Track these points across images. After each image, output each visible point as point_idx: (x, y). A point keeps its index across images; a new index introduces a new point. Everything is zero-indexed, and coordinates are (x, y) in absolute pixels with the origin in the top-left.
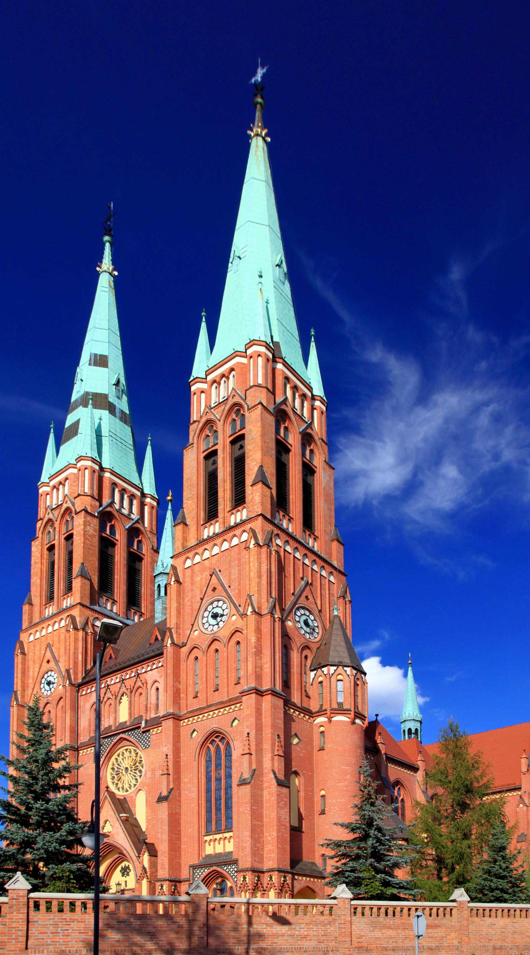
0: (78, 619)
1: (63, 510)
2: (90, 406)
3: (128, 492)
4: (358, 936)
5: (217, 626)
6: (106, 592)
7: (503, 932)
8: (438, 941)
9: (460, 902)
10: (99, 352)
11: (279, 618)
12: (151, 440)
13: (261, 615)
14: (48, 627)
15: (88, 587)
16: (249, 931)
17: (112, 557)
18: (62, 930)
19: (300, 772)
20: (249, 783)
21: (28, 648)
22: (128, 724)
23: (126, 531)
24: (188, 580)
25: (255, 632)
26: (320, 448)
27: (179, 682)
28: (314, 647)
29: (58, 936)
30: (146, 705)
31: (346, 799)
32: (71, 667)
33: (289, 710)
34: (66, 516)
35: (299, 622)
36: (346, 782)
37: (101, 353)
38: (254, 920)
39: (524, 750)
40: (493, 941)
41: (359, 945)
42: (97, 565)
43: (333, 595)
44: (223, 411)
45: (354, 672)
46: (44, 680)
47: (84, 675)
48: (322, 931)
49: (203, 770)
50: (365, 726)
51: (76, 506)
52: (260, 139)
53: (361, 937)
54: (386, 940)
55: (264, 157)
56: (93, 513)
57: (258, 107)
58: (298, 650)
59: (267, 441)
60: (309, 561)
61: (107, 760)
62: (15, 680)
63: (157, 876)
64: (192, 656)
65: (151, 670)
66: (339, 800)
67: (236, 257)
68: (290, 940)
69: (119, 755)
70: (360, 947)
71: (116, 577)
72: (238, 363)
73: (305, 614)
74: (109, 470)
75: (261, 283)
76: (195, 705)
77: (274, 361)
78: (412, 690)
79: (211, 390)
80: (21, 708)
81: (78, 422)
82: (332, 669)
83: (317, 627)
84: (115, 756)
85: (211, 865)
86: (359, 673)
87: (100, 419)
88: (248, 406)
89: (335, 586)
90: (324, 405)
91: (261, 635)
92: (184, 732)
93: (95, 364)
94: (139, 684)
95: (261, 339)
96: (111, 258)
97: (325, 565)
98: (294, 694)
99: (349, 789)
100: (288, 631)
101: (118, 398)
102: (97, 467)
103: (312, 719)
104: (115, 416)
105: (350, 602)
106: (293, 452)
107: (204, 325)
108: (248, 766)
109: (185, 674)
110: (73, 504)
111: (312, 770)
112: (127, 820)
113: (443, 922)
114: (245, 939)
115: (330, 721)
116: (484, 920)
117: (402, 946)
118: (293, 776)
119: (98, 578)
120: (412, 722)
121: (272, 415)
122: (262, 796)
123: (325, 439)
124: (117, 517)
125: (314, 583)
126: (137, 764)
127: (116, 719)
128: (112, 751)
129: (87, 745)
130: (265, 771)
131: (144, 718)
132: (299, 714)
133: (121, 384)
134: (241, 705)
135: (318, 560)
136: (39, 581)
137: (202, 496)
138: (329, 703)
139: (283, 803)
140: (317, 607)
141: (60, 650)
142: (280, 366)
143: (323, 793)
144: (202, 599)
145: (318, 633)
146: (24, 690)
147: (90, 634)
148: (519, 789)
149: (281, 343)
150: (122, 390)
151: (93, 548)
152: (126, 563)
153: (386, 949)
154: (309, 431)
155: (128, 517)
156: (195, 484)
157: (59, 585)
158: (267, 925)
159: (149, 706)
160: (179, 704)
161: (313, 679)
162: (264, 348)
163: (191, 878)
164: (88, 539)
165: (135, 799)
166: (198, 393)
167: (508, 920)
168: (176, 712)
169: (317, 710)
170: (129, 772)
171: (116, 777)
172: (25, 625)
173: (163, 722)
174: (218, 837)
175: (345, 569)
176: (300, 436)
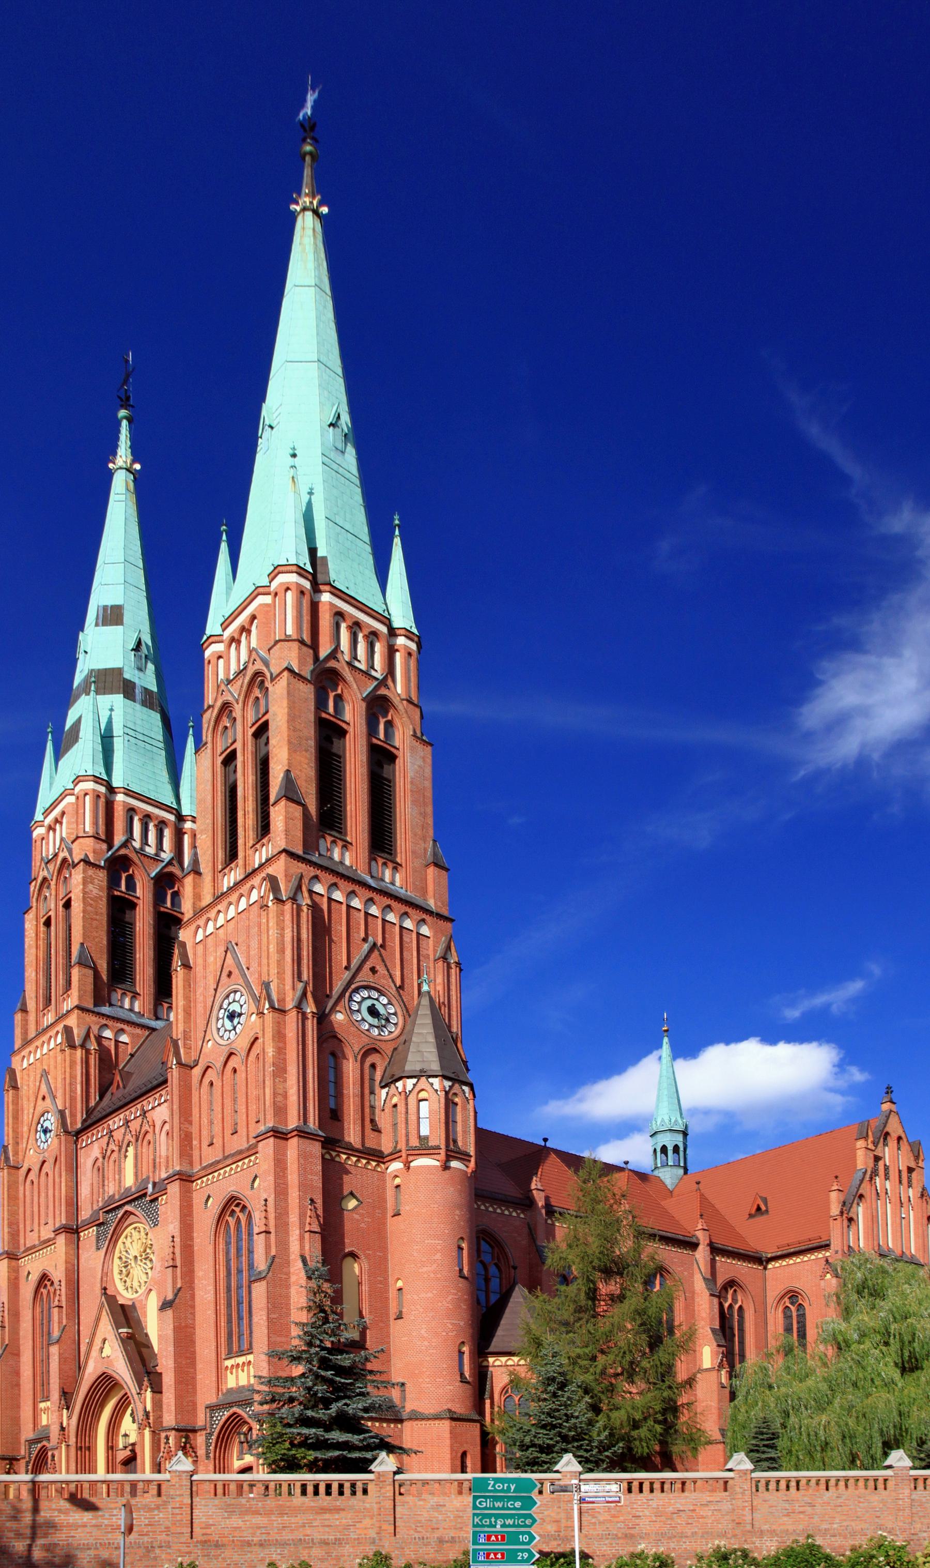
0: (75, 1031)
1: (59, 862)
2: (92, 693)
3: (154, 818)
4: (203, 1525)
5: (233, 1032)
6: (123, 981)
9: (379, 1473)
10: (110, 603)
11: (313, 1013)
12: (193, 727)
13: (285, 1012)
14: (43, 1045)
15: (90, 980)
16: (34, 1520)
17: (132, 924)
19: (359, 1253)
20: (264, 1278)
21: (22, 1078)
22: (133, 1190)
23: (152, 882)
24: (200, 961)
25: (273, 1040)
26: (405, 715)
27: (191, 1123)
28: (388, 1049)
30: (154, 1160)
31: (435, 1292)
32: (67, 1105)
33: (338, 1155)
34: (65, 870)
35: (358, 1011)
36: (435, 1266)
37: (113, 603)
38: (43, 1504)
39: (836, 1177)
40: (441, 1530)
41: (204, 1538)
42: (105, 942)
43: (428, 957)
45: (447, 1084)
46: (40, 1126)
47: (85, 1116)
49: (221, 1257)
50: (469, 1171)
51: (74, 855)
52: (309, 214)
53: (208, 1526)
54: (250, 1531)
55: (315, 244)
56: (97, 863)
57: (308, 159)
58: (356, 1057)
59: (298, 727)
60: (378, 908)
61: (111, 1245)
62: (6, 1128)
63: (162, 1422)
64: (206, 1081)
65: (159, 1105)
66: (423, 1295)
67: (267, 427)
68: (95, 1532)
69: (126, 1237)
70: (205, 1542)
71: (138, 956)
72: (261, 605)
73: (369, 997)
74: (122, 790)
75: (293, 467)
76: (211, 1155)
77: (316, 588)
78: (668, 1078)
79: (229, 653)
80: (13, 1171)
81: (79, 721)
82: (410, 1083)
83: (395, 1014)
84: (122, 1239)
85: (230, 1405)
86: (457, 1085)
87: (111, 710)
88: (271, 674)
89: (431, 941)
90: (412, 640)
91: (285, 1043)
92: (198, 1199)
93: (105, 623)
94: (146, 1127)
95: (290, 563)
96: (129, 443)
97: (409, 910)
98: (349, 1128)
99: (439, 1276)
100: (336, 1030)
101: (140, 669)
102: (102, 789)
103: (382, 1165)
104: (135, 701)
105: (458, 964)
106: (352, 734)
107: (224, 547)
108: (264, 1252)
109: (198, 1110)
110: (71, 854)
111: (384, 1249)
112: (129, 1338)
113: (350, 1503)
114: (28, 1532)
115: (407, 1167)
117: (277, 1540)
118: (349, 1260)
119: (108, 963)
120: (668, 1134)
121: (309, 681)
122: (288, 1297)
123: (415, 699)
124: (137, 861)
125: (388, 943)
126: (148, 1251)
127: (120, 1182)
128: (117, 1231)
129: (88, 1224)
130: (292, 1257)
131: (151, 1180)
132: (358, 1161)
133: (144, 647)
134: (256, 1158)
135: (394, 904)
136: (34, 974)
137: (219, 825)
138: (404, 1139)
140: (394, 982)
141: (57, 1080)
142: (326, 597)
143: (400, 1284)
144: (216, 990)
145: (395, 1024)
146: (17, 1143)
147: (93, 1052)
148: (826, 1246)
149: (329, 559)
150: (146, 656)
151: (98, 917)
152: (152, 931)
153: (249, 1544)
154: (383, 691)
155: (156, 859)
156: (210, 807)
157: (58, 981)
158: (60, 1511)
159: (158, 1160)
160: (191, 1156)
162: (295, 575)
163: (208, 1425)
164: (91, 905)
165: (146, 1305)
166: (213, 661)
168: (186, 1168)
169: (390, 1150)
170: (139, 1262)
171: (124, 1270)
172: (18, 1043)
173: (169, 1186)
174: (240, 1360)
175: (450, 910)
176: (364, 705)
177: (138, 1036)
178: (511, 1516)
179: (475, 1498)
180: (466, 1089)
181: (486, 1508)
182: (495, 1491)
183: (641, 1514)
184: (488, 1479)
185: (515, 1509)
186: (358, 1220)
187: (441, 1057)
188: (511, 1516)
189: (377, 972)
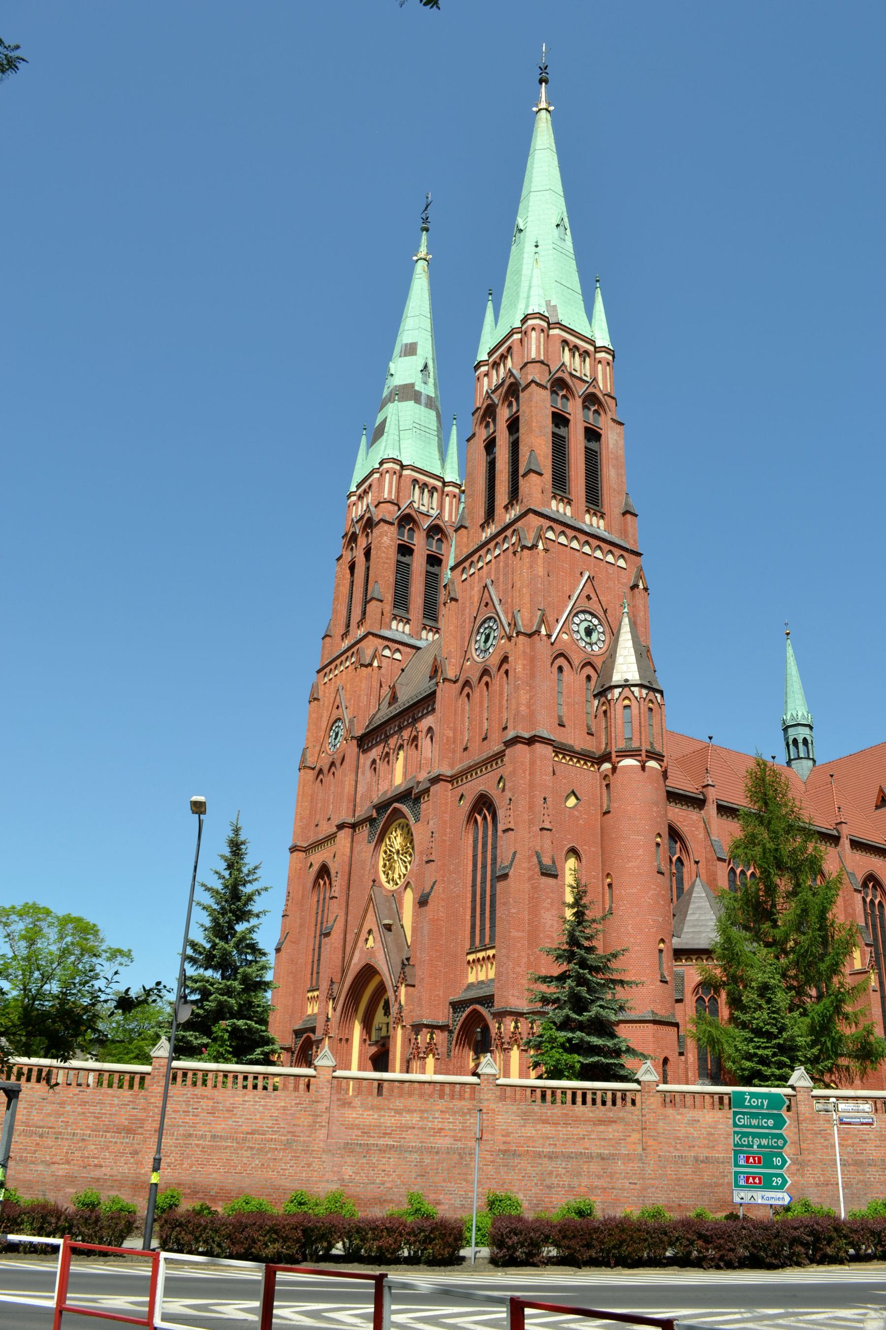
4: (504, 1133)
7: (712, 1134)
8: (613, 1146)
18: (193, 1109)
29: (189, 1116)
35: (578, 631)
36: (638, 861)
41: (504, 1147)
44: (501, 394)
48: (460, 1123)
70: (506, 1151)
86: (651, 693)
93: (405, 355)
101: (425, 383)
104: (420, 404)
116: (681, 1114)
139: (549, 901)
161: (597, 707)
167: (720, 1114)
171: (387, 863)
174: (481, 955)
177: (408, 653)
178: (765, 1136)
179: (736, 1114)
180: (658, 696)
181: (743, 1126)
182: (751, 1107)
183: (867, 1137)
184: (744, 1093)
185: (768, 1127)
186: (577, 817)
187: (640, 669)
188: (765, 1136)
189: (591, 599)
